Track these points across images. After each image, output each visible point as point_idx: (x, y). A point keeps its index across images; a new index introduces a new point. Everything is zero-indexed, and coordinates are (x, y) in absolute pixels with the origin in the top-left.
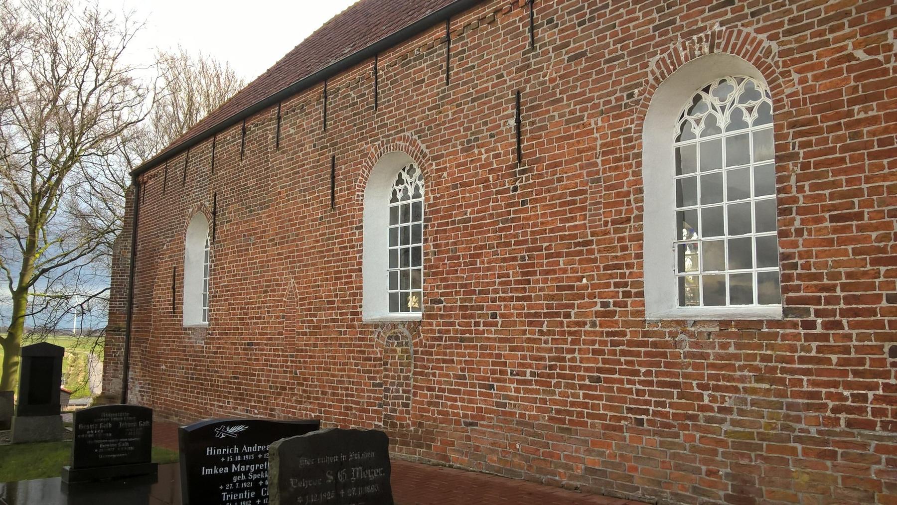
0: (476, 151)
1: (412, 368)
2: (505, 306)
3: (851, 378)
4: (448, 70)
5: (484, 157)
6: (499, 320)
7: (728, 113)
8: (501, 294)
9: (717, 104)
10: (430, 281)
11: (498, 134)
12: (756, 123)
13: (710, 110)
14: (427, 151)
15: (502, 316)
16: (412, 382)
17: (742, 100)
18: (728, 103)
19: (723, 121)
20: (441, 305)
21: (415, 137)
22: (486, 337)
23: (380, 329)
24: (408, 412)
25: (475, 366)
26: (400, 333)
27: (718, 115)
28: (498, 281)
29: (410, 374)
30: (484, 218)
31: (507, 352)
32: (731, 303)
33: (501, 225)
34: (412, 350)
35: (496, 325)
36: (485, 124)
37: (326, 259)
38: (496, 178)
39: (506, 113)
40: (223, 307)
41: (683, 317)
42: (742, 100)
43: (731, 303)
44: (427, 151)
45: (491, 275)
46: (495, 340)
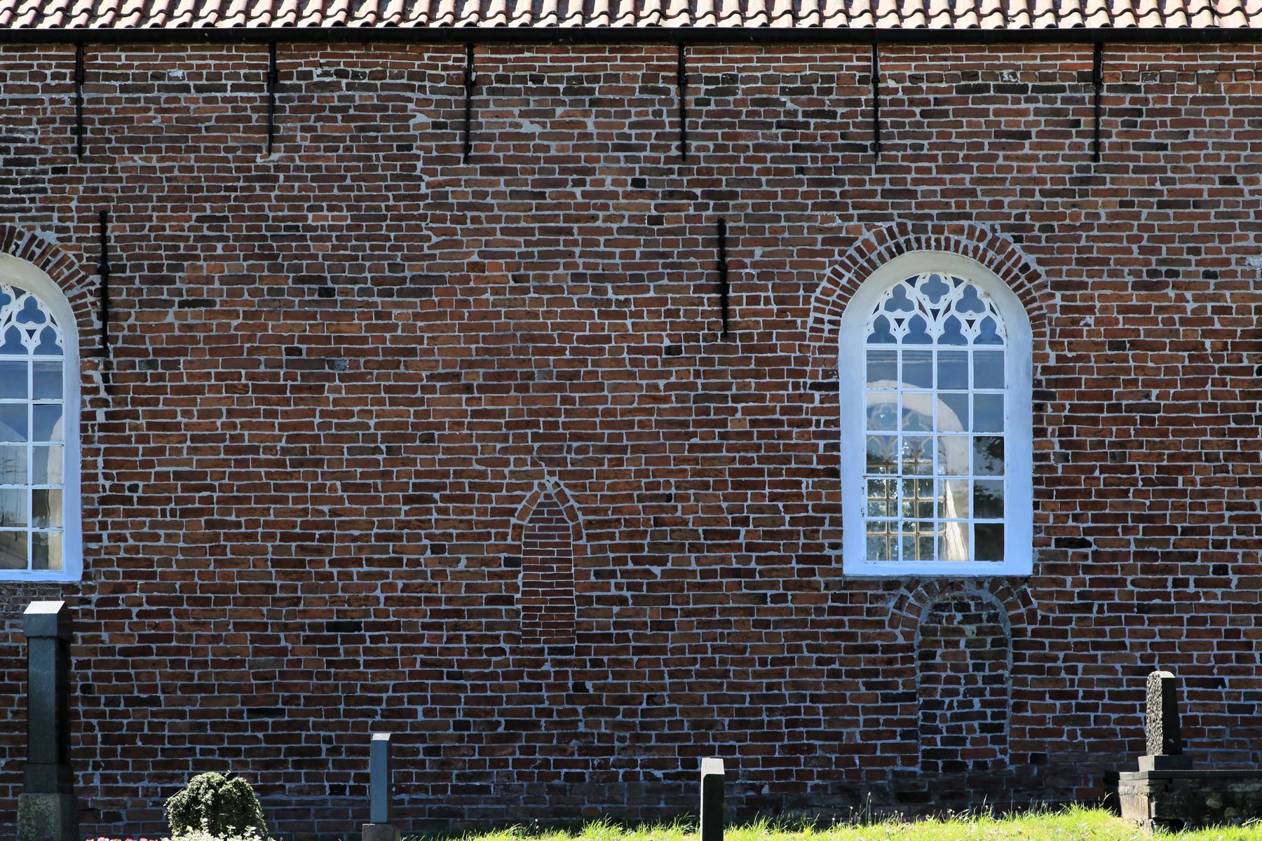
0: (1171, 293)
1: (1009, 661)
2: (1245, 555)
3: (630, 566)
4: (1097, 134)
5: (1191, 306)
6: (1234, 578)
7: (942, 319)
8: (1235, 536)
9: (928, 306)
10: (1053, 506)
11: (1223, 274)
12: (906, 340)
13: (917, 311)
14: (1041, 270)
15: (1238, 570)
16: (1009, 686)
17: (961, 307)
18: (941, 306)
19: (935, 328)
20: (1088, 551)
21: (1008, 236)
22: (1203, 605)
23: (903, 591)
24: (1002, 741)
25: (1178, 651)
26: (973, 598)
27: (929, 319)
28: (1227, 514)
29: (1006, 674)
30: (1193, 408)
31: (1252, 627)
32: (976, 525)
33: (1233, 425)
34: (1007, 627)
35: (1227, 583)
36: (1196, 251)
37: (693, 441)
38: (1220, 346)
39: (1239, 244)
40: (1006, 584)
41: (966, 538)
42: (961, 307)
43: (976, 525)
44: (1041, 270)
45: (1210, 504)
46: (1225, 608)
